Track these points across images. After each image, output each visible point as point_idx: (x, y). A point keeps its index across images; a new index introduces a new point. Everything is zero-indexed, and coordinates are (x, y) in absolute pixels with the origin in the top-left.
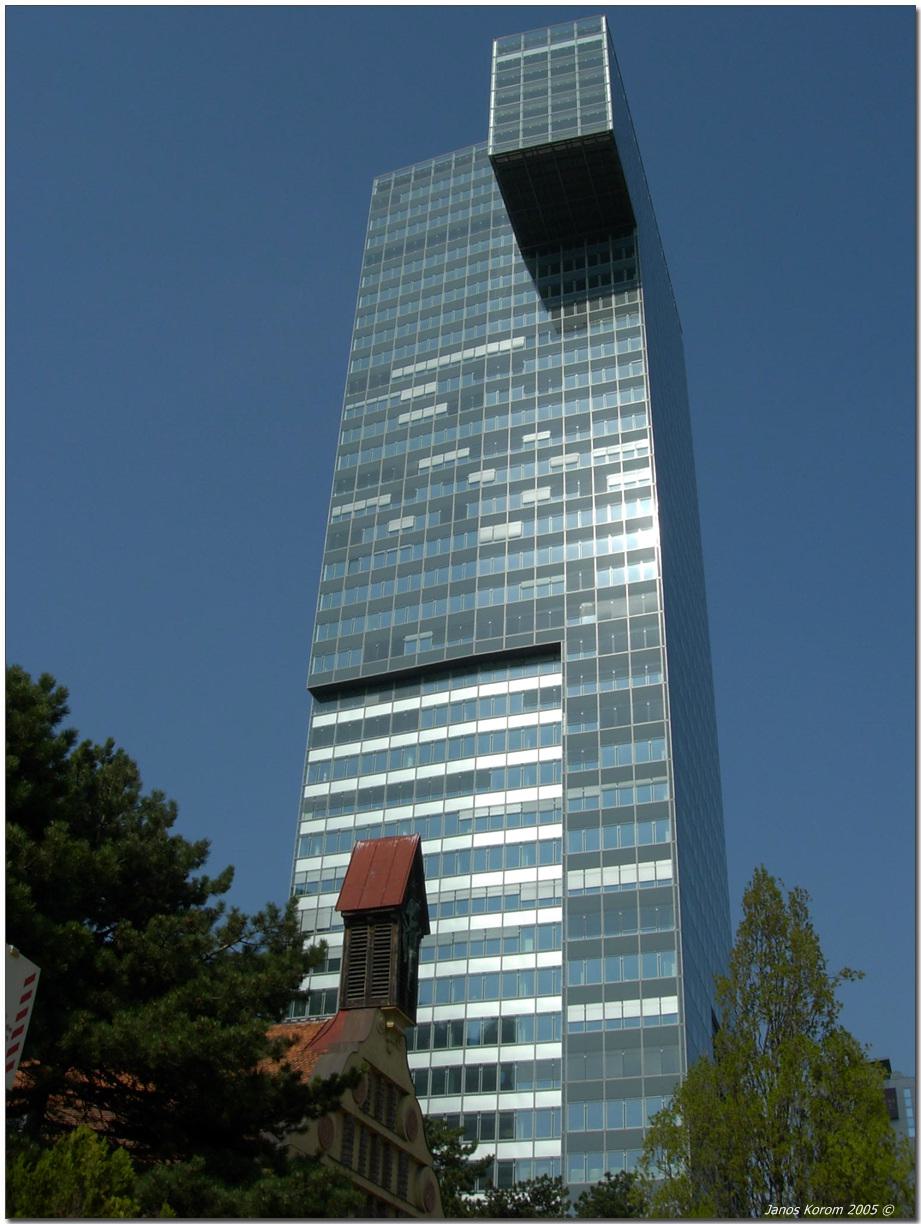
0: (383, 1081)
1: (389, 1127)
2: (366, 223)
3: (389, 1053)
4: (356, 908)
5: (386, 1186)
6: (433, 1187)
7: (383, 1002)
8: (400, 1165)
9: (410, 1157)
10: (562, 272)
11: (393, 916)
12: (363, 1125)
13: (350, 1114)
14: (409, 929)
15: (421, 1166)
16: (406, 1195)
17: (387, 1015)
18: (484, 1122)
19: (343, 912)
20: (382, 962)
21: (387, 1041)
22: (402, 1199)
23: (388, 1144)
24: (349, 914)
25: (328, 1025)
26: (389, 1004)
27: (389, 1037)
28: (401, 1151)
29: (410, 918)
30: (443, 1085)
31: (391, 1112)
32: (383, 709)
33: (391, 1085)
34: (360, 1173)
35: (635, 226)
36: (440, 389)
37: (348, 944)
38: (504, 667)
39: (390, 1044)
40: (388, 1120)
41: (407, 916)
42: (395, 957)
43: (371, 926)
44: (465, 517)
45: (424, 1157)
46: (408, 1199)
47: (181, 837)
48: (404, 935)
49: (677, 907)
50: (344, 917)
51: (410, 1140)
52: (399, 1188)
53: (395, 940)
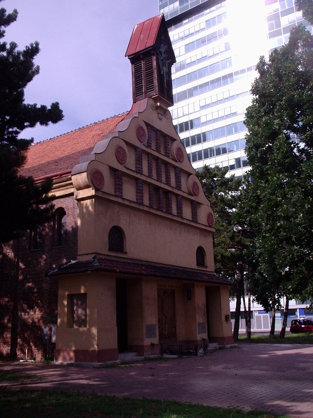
0: (158, 133)
1: (167, 155)
3: (160, 119)
4: (134, 52)
5: (168, 183)
6: (196, 184)
7: (152, 94)
8: (176, 174)
9: (182, 170)
11: (152, 52)
13: (138, 147)
14: (162, 58)
17: (155, 100)
18: (192, 140)
19: (128, 56)
20: (150, 74)
21: (158, 114)
22: (178, 190)
23: (166, 163)
24: (131, 57)
25: (177, 131)
26: (155, 93)
27: (159, 112)
28: (175, 167)
29: (163, 53)
30: (183, 129)
31: (166, 148)
34: (150, 176)
37: (133, 72)
40: (166, 152)
41: (161, 52)
42: (155, 72)
43: (143, 60)
44: (200, 3)
47: (17, 10)
48: (160, 61)
49: (49, 372)
50: (129, 59)
51: (179, 161)
52: (176, 184)
53: (155, 63)
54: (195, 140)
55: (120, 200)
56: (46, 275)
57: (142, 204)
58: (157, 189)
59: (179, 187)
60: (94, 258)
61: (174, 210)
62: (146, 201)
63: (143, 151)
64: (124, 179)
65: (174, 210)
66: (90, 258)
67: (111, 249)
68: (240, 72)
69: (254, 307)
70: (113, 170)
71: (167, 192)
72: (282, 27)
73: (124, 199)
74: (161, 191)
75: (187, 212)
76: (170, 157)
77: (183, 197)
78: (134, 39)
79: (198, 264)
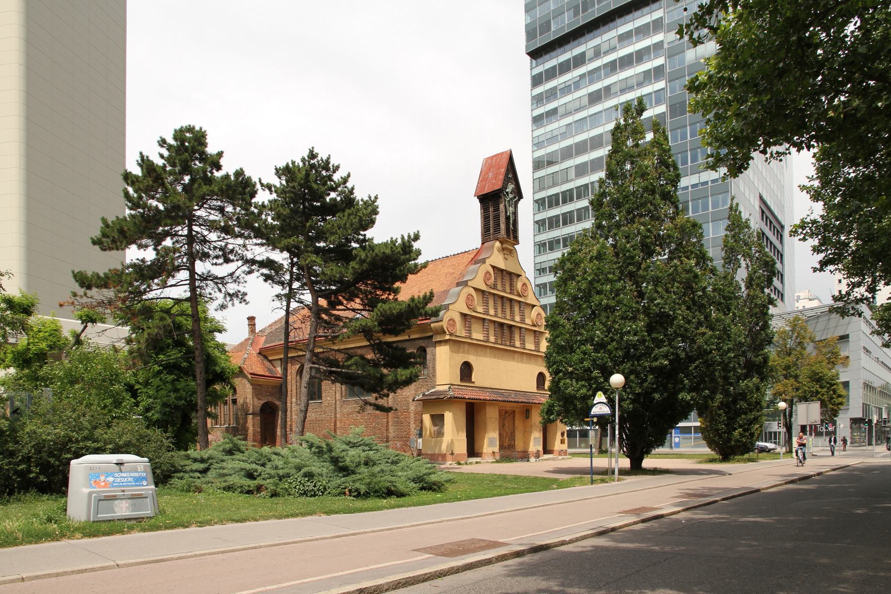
20: (497, 218)
40: (511, 289)
54: (552, 223)
55: (469, 341)
56: (413, 400)
57: (488, 341)
58: (502, 325)
59: (523, 321)
60: (450, 388)
61: (518, 344)
62: (492, 339)
63: (490, 293)
64: (473, 320)
65: (518, 344)
66: (446, 388)
67: (462, 380)
68: (635, 87)
69: (100, 502)
70: (464, 315)
71: (510, 327)
72: (686, 64)
73: (472, 339)
74: (505, 326)
75: (530, 346)
76: (515, 293)
77: (526, 329)
78: (483, 178)
79: (538, 388)
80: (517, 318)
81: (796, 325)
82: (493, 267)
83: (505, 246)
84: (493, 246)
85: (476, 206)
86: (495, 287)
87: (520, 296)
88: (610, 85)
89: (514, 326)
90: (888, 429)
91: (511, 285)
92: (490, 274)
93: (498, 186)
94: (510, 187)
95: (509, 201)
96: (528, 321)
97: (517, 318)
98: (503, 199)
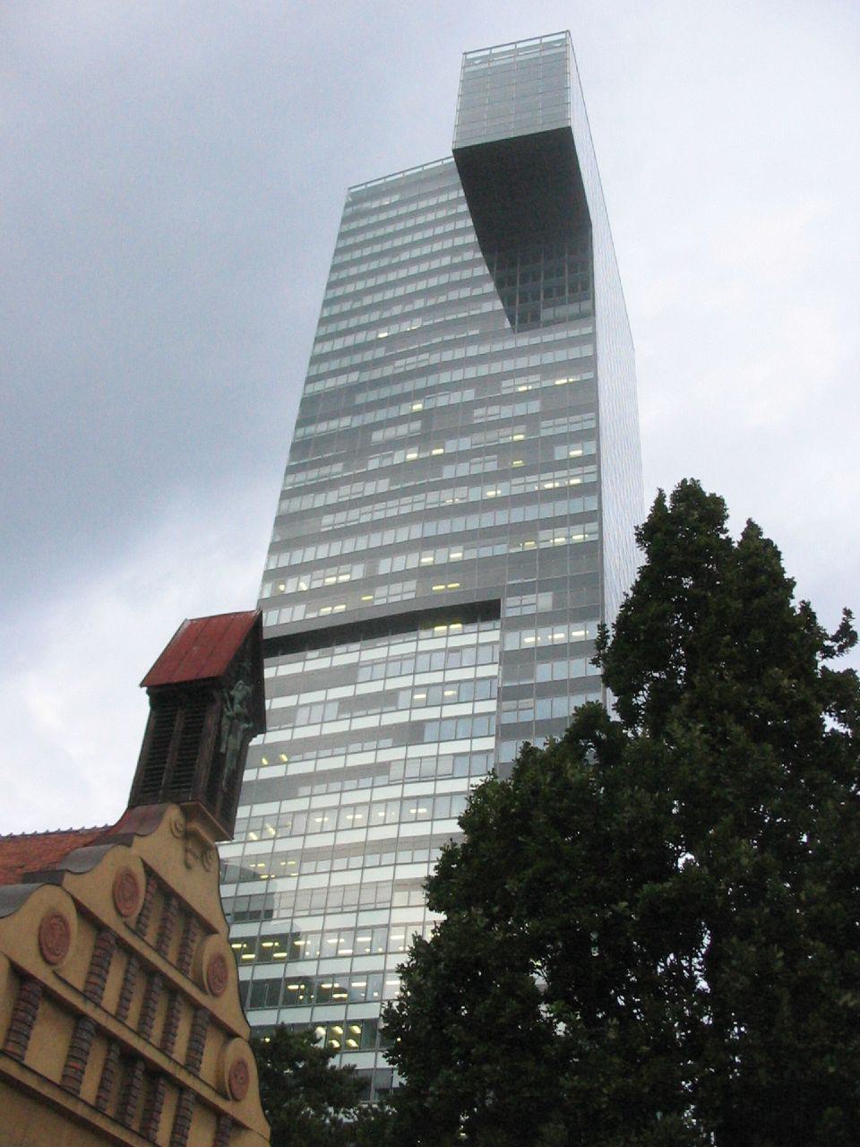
1: (181, 966)
2: (548, 489)
5: (165, 1048)
10: (567, 294)
12: (130, 952)
15: (231, 1035)
16: (198, 1070)
21: (187, 851)
23: (173, 991)
28: (196, 1007)
29: (236, 701)
32: (574, 333)
33: (188, 912)
35: (779, 554)
36: (556, 602)
38: (355, 640)
39: (190, 856)
41: (232, 699)
45: (235, 1023)
46: (201, 1075)
52: (188, 1056)
57: (74, 1094)
58: (130, 1057)
59: (192, 1065)
64: (44, 1008)
74: (141, 1065)
76: (190, 975)
80: (180, 1048)
81: (132, 1117)
82: (149, 872)
83: (195, 826)
84: (160, 815)
85: (139, 709)
86: (139, 932)
87: (201, 988)
88: (390, 762)
89: (183, 992)
90: (163, 1133)
91: (184, 947)
92: (135, 884)
93: (214, 668)
94: (240, 691)
95: (231, 719)
96: (207, 1068)
97: (180, 1048)
98: (215, 707)
